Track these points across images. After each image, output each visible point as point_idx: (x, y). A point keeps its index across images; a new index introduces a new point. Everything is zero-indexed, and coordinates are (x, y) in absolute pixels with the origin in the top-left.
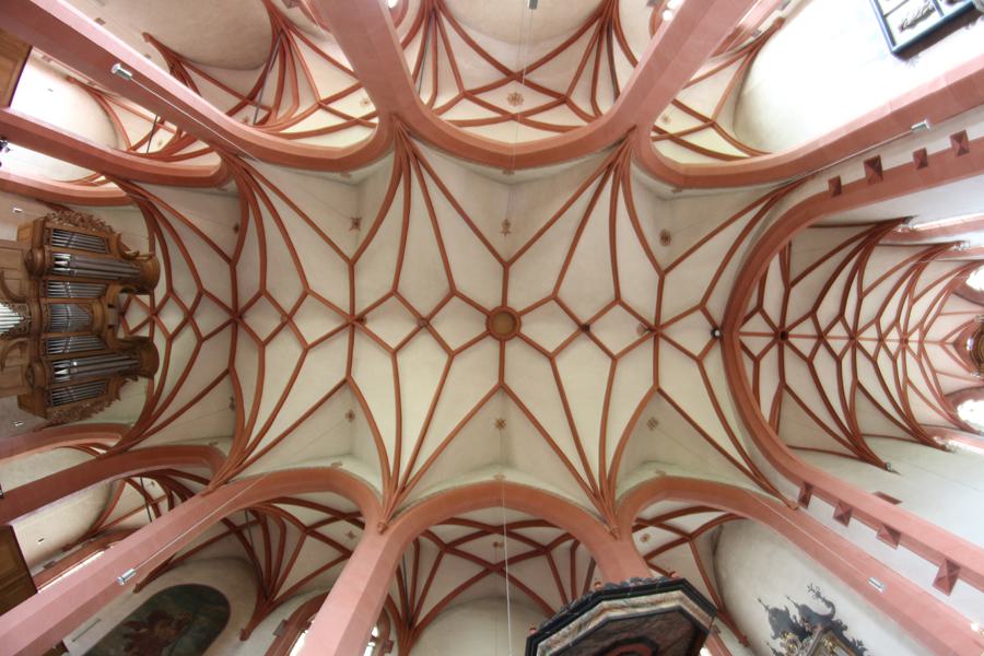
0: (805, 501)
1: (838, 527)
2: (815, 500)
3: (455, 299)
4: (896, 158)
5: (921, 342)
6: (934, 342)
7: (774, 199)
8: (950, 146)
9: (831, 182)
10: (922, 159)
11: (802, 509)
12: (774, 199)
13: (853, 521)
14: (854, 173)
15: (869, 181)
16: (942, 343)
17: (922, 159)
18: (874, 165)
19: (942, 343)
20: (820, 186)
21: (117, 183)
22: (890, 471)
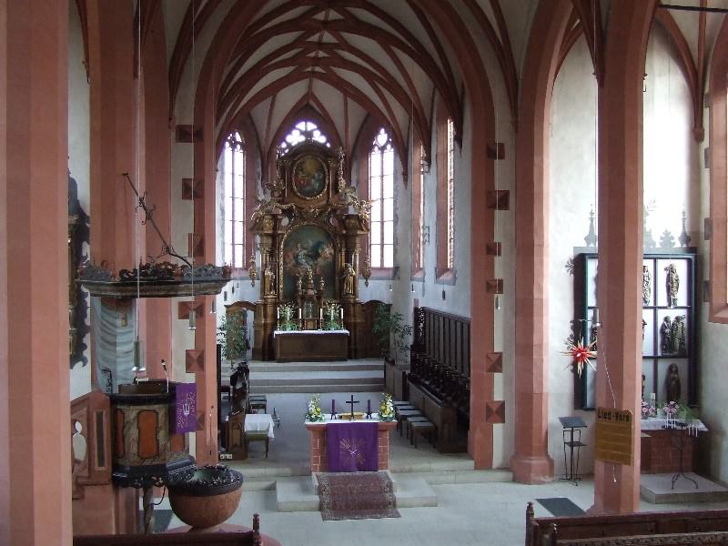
0: (183, 134)
1: (176, 189)
2: (189, 148)
3: (659, 261)
4: (503, 223)
5: (314, 74)
6: (310, 87)
7: (504, 54)
8: (495, 399)
9: (501, 282)
10: (492, 250)
11: (173, 134)
12: (504, 54)
13: (191, 204)
14: (503, 177)
15: (490, 192)
16: (310, 95)
17: (492, 250)
18: (504, 203)
19: (310, 95)
20: (502, 134)
21: (84, 336)
22: (279, 511)
